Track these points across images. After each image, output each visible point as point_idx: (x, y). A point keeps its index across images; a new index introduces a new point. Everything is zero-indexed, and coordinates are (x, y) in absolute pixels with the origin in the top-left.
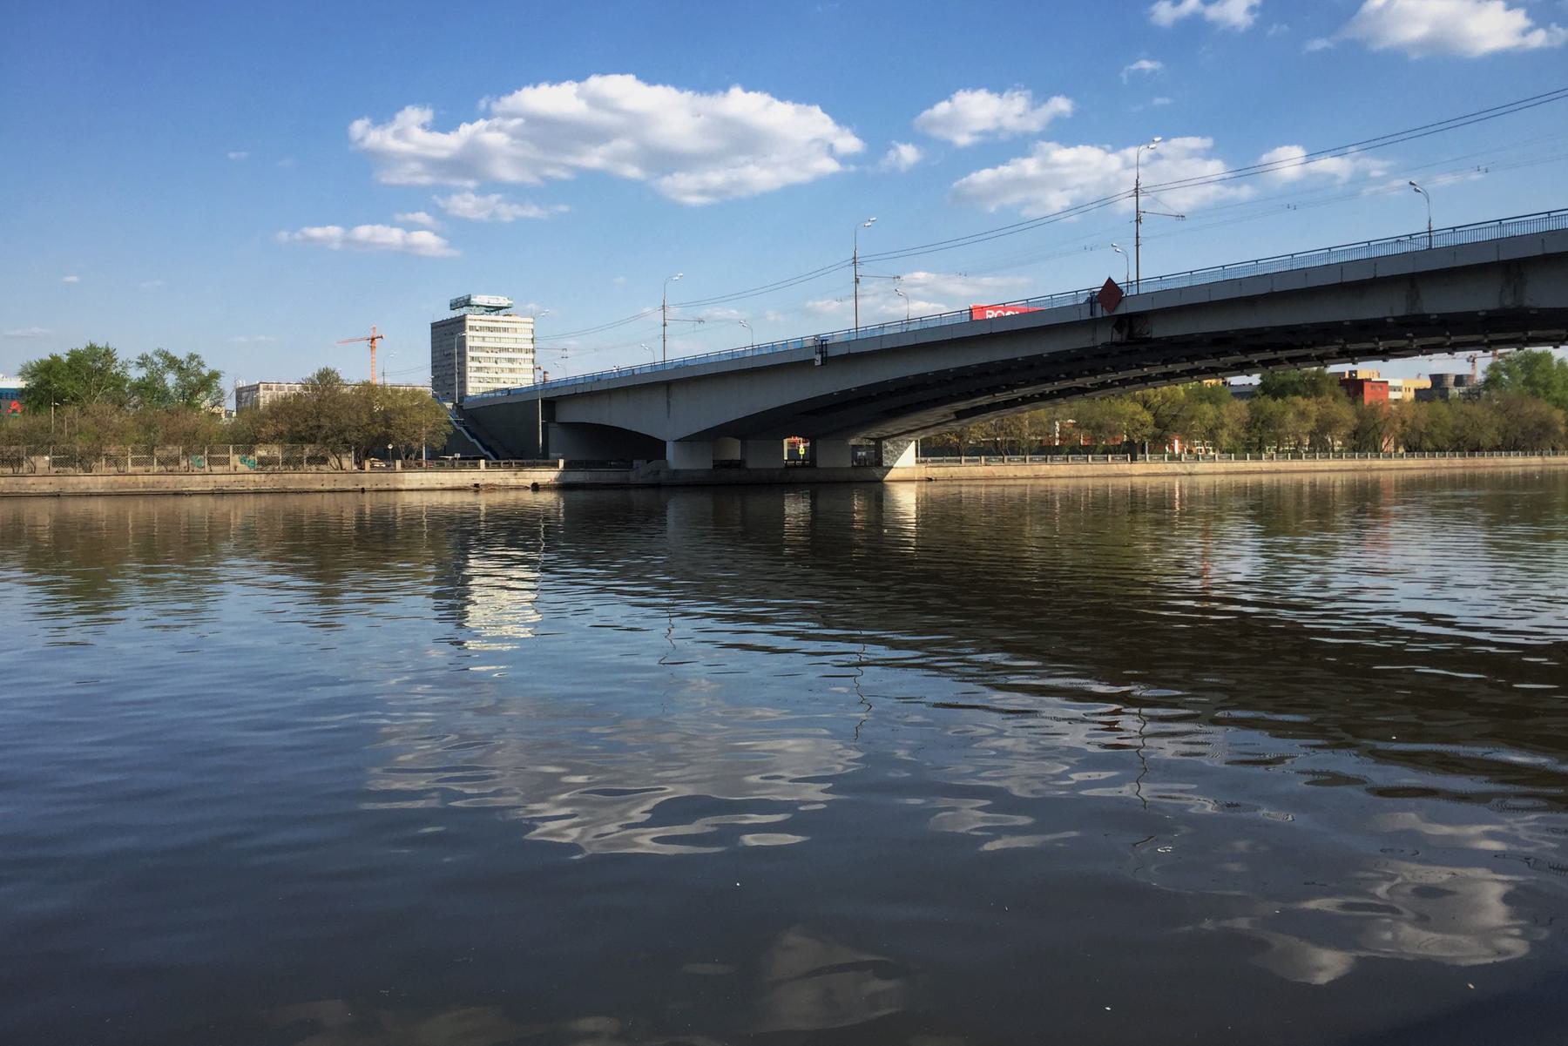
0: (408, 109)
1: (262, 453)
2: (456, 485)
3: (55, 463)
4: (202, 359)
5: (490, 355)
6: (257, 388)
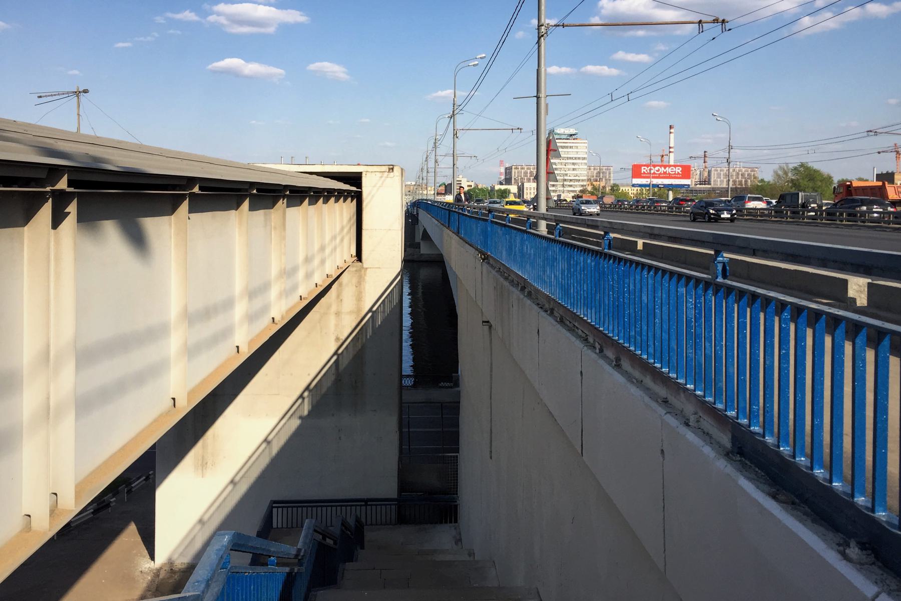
0: (620, 52)
4: (836, 179)
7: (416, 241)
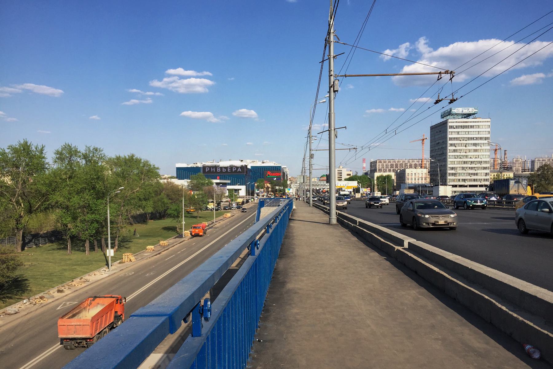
5: (462, 142)
6: (376, 162)
7: (408, 248)
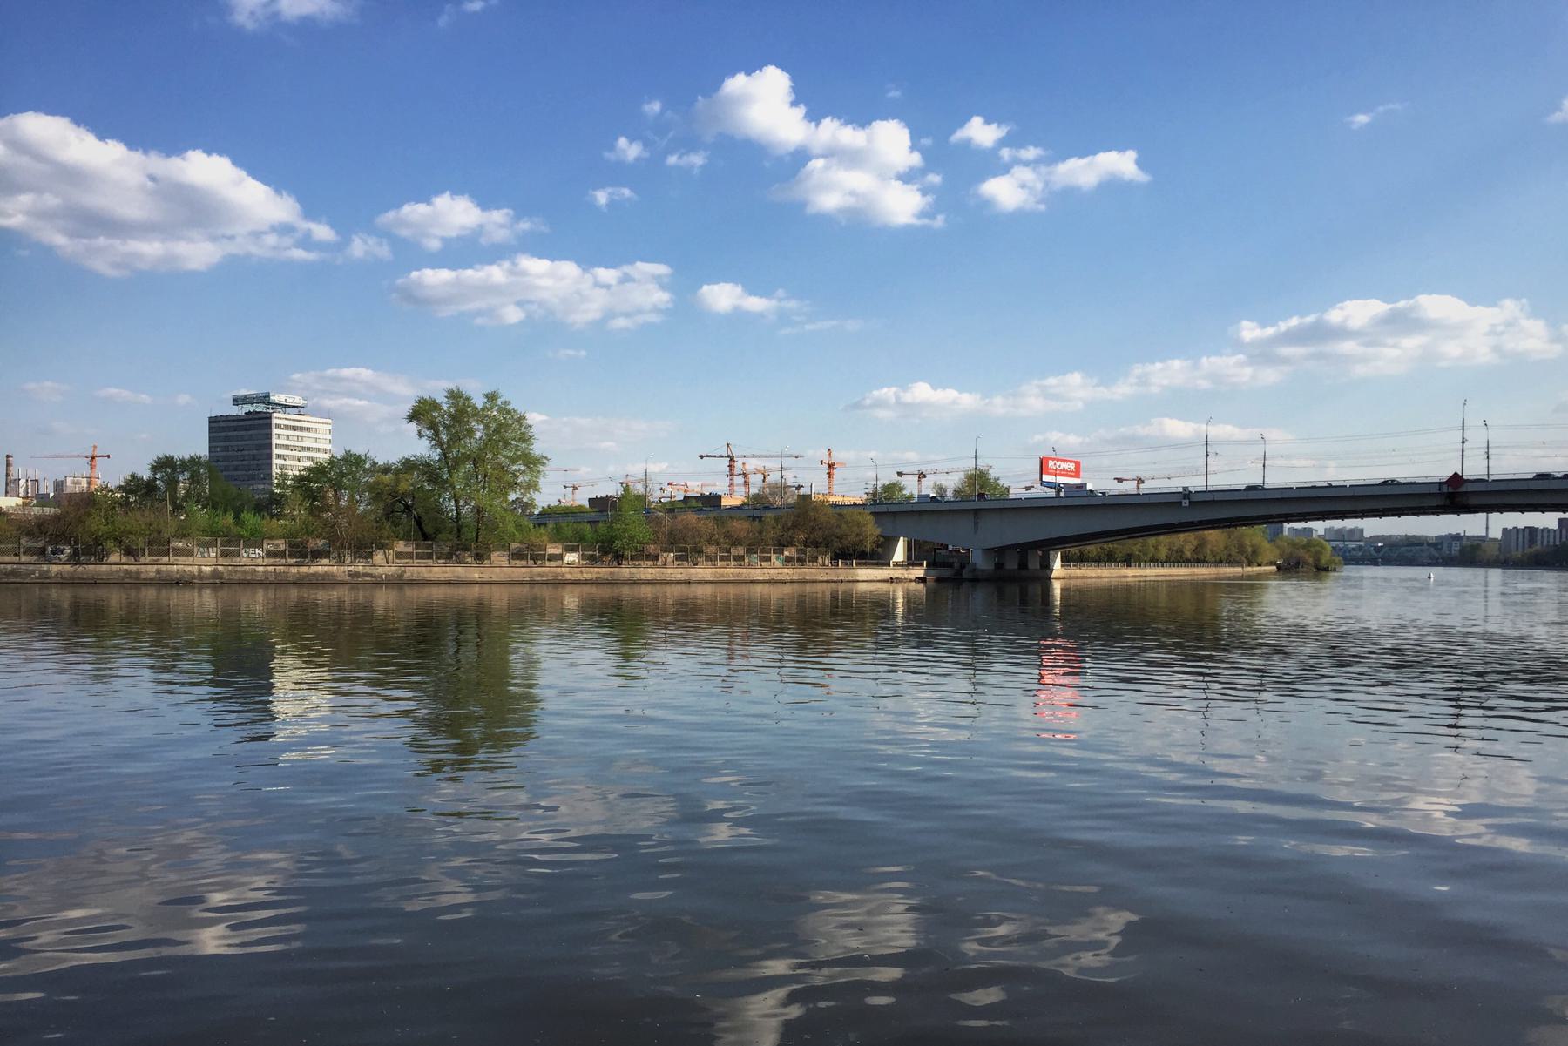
1: (786, 553)
2: (883, 578)
3: (677, 558)
5: (294, 453)
7: (1500, 538)
